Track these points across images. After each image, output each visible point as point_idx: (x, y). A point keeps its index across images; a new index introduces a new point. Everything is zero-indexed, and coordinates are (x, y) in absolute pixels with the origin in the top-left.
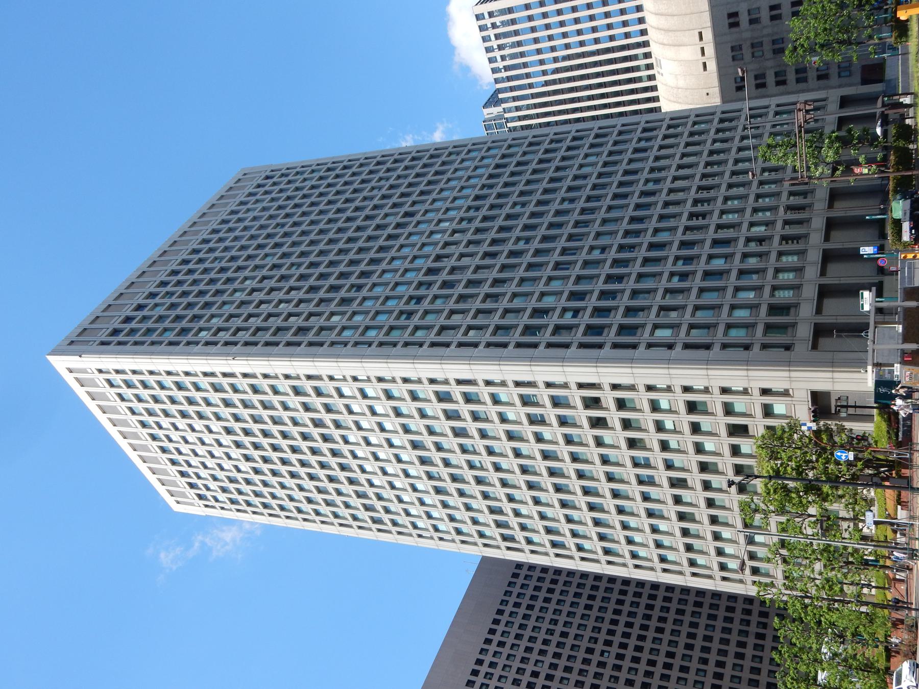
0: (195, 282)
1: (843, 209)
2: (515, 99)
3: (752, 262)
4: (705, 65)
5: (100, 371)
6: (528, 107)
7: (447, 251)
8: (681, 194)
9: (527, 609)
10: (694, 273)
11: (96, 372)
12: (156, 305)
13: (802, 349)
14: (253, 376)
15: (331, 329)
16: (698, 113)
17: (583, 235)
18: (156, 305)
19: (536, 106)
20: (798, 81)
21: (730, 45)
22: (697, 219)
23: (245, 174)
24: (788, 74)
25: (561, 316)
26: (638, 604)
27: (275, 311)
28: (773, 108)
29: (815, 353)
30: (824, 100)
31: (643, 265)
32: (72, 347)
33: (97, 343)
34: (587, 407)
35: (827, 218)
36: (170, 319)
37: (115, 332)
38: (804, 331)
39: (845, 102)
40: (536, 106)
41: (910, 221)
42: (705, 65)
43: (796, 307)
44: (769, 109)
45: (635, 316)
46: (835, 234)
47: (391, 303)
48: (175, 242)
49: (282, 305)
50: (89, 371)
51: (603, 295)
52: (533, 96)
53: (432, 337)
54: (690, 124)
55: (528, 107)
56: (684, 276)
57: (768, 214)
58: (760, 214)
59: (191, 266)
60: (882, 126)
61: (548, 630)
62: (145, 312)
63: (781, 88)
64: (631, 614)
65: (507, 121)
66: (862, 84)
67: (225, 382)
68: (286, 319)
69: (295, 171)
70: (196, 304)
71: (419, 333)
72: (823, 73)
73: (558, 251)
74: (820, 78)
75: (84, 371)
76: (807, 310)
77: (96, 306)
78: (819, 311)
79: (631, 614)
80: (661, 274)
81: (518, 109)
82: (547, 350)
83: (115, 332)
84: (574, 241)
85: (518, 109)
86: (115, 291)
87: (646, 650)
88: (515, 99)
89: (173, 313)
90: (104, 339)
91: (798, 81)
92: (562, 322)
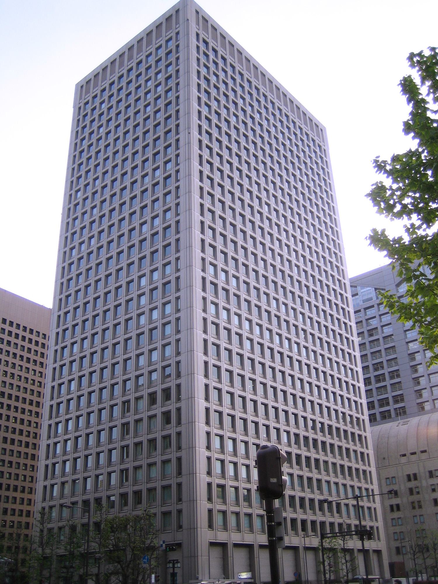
4: (404, 455)
5: (178, 33)
9: (23, 336)
11: (177, 30)
14: (177, 52)
20: (392, 506)
21: (417, 472)
23: (322, 130)
24: (398, 512)
26: (28, 436)
30: (379, 539)
33: (198, 31)
34: (164, 437)
37: (206, 42)
39: (378, 552)
42: (404, 455)
44: (372, 503)
48: (272, 83)
50: (177, 26)
53: (209, 278)
54: (356, 399)
63: (388, 509)
64: (22, 421)
66: (389, 563)
67: (172, 187)
69: (323, 156)
71: (213, 307)
72: (401, 551)
74: (398, 549)
75: (177, 23)
76: (236, 538)
78: (236, 545)
79: (21, 432)
82: (202, 318)
83: (206, 42)
90: (201, 36)
91: (392, 506)
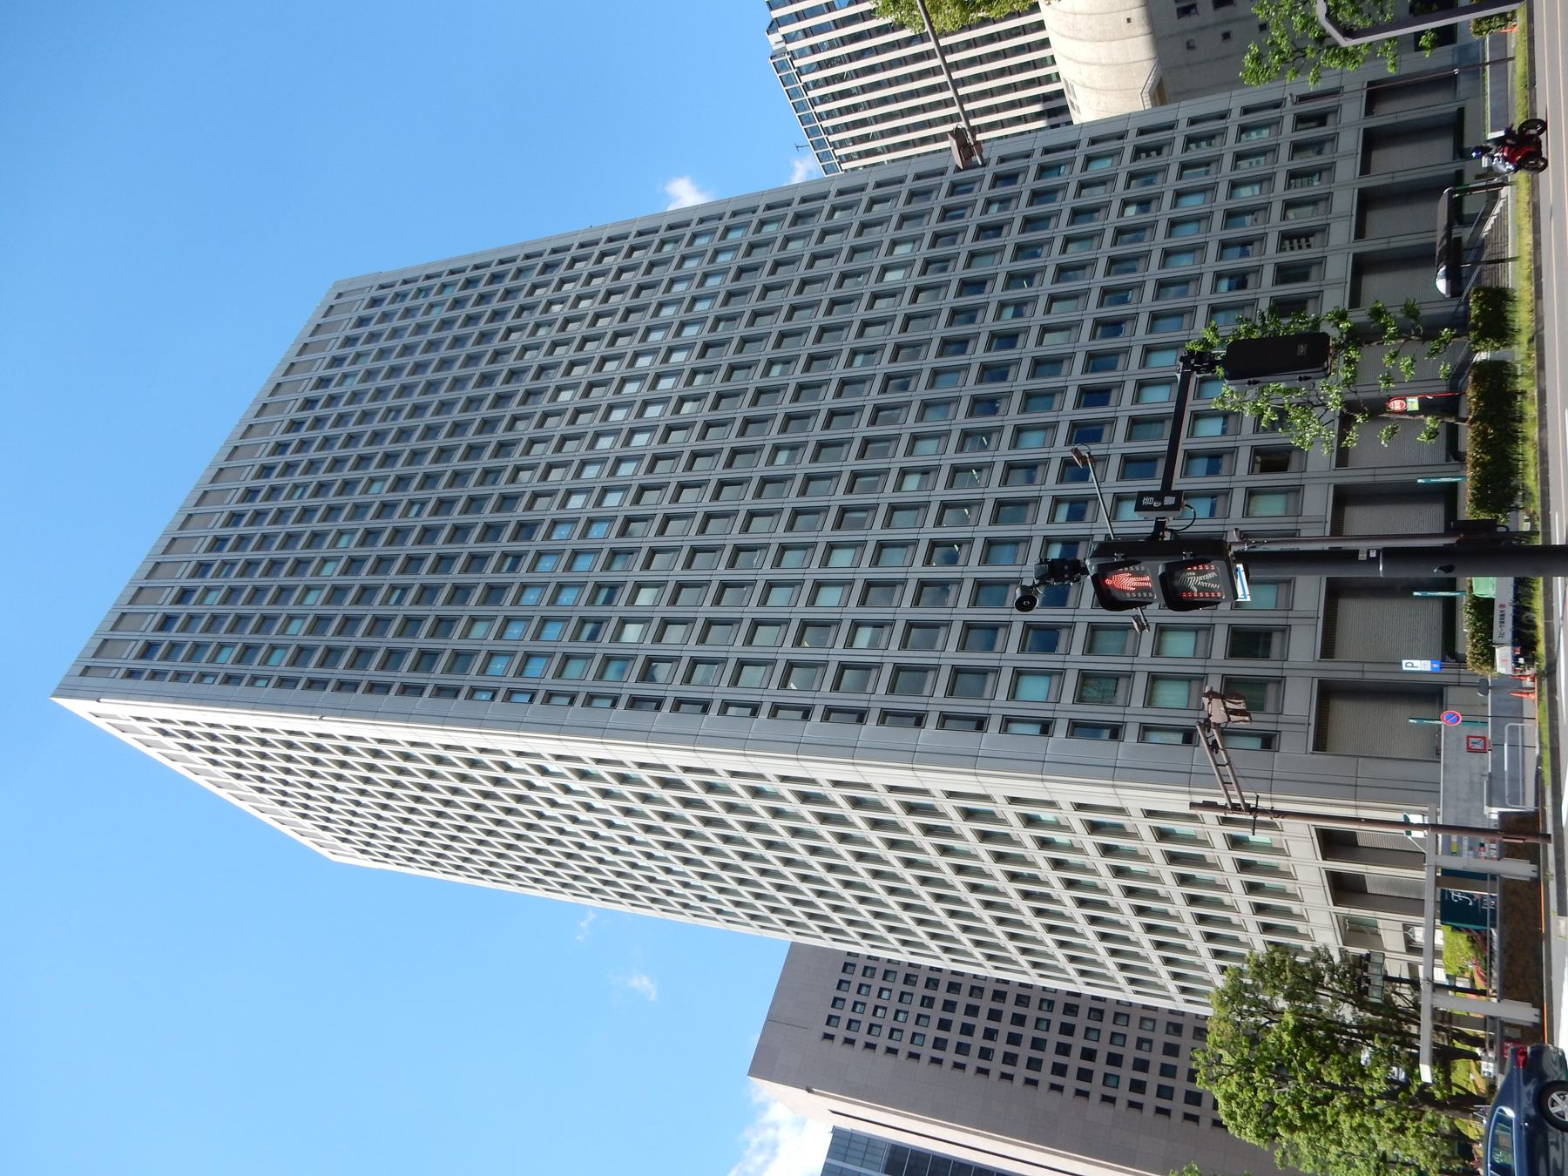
0: (395, 333)
1: (1392, 113)
2: (807, 33)
3: (1247, 194)
6: (832, 45)
7: (744, 282)
8: (1099, 190)
10: (1159, 196)
12: (345, 376)
13: (1296, 744)
15: (665, 262)
16: (1095, 133)
17: (964, 207)
18: (345, 376)
19: (844, 41)
22: (1148, 155)
23: (340, 295)
25: (985, 211)
27: (532, 341)
28: (1236, 119)
29: (1321, 757)
31: (1072, 221)
32: (87, 681)
33: (122, 672)
35: (1360, 191)
36: (354, 419)
38: (1299, 701)
40: (844, 41)
41: (1514, 644)
43: (1283, 631)
45: (1091, 220)
46: (1376, 218)
47: (712, 282)
49: (528, 355)
51: (1013, 279)
52: (837, 24)
55: (832, 45)
56: (1144, 204)
57: (1265, 132)
58: (1254, 135)
59: (385, 307)
60: (1448, 276)
61: (924, 998)
62: (332, 389)
65: (800, 72)
68: (551, 352)
70: (415, 346)
73: (936, 214)
77: (83, 645)
80: (1100, 234)
81: (815, 49)
84: (954, 218)
85: (815, 49)
86: (256, 401)
87: (1079, 1032)
88: (807, 33)
89: (372, 386)
92: (986, 219)
